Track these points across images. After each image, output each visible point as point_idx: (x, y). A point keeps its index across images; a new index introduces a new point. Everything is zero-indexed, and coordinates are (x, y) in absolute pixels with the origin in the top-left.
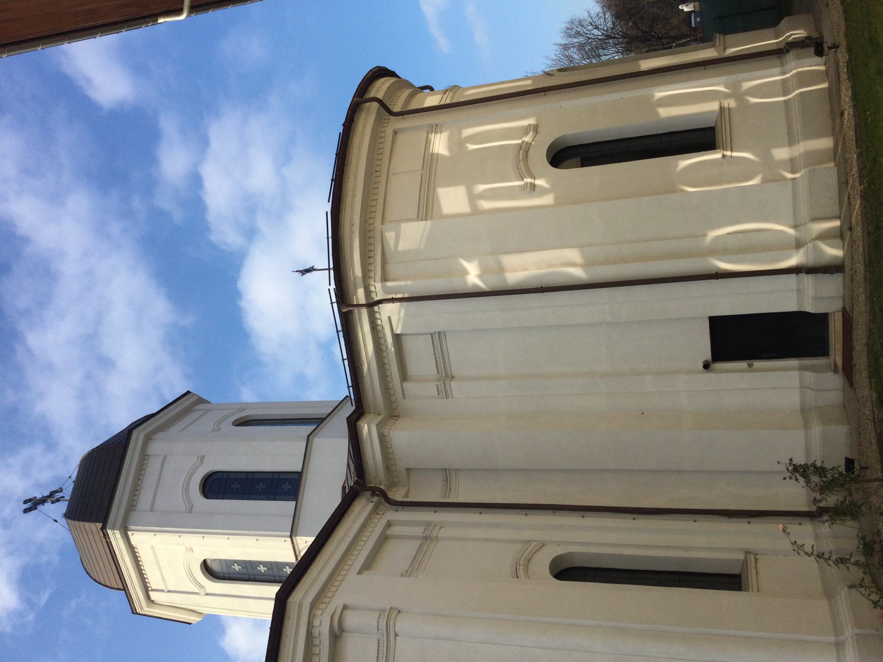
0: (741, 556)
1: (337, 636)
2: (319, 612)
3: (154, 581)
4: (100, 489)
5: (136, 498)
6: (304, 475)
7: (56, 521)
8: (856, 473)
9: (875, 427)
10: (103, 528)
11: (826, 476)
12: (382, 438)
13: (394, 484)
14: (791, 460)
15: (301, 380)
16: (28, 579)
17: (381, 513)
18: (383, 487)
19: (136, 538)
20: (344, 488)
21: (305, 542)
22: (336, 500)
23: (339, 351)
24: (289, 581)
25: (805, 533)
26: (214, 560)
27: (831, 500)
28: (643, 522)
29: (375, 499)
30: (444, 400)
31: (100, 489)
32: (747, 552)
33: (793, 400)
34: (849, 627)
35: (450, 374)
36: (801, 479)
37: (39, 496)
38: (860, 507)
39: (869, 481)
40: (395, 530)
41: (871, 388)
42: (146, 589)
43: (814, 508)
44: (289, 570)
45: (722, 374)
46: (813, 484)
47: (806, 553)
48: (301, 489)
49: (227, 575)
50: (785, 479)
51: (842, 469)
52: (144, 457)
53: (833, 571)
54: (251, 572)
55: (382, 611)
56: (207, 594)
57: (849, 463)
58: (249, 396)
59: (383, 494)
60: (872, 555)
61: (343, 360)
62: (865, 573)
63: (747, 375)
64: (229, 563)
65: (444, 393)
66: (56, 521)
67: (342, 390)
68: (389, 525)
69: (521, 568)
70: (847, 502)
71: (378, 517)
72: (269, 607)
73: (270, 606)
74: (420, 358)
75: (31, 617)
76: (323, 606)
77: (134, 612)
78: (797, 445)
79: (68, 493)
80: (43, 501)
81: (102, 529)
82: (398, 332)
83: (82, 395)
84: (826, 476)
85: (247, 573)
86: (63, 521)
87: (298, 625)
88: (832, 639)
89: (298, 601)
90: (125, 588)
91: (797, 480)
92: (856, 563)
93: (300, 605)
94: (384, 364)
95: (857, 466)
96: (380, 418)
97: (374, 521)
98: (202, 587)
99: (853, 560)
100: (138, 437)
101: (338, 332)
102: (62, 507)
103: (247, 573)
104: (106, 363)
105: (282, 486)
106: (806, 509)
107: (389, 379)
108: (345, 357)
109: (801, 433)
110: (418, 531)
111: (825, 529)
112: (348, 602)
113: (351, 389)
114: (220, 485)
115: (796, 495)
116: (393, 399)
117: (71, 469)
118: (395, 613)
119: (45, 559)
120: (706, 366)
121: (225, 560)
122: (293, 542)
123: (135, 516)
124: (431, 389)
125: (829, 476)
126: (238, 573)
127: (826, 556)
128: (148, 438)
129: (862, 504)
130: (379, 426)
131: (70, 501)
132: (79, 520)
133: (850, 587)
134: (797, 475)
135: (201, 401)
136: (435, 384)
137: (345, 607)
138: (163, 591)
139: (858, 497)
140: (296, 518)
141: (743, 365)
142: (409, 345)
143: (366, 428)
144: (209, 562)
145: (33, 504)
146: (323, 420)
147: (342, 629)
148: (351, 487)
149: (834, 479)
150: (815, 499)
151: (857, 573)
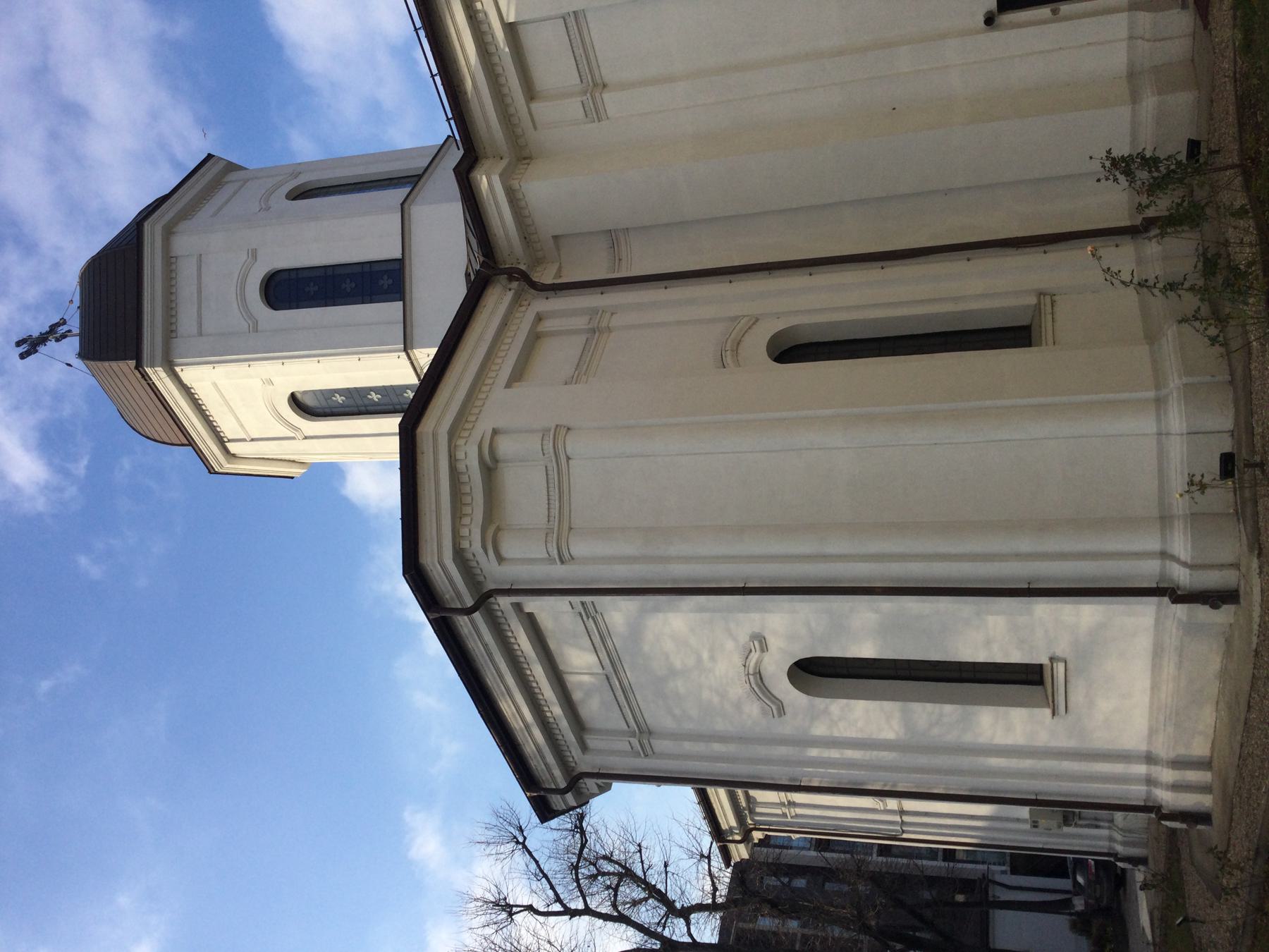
0: (1032, 300)
1: (490, 468)
2: (461, 442)
3: (228, 428)
4: (118, 310)
5: (174, 320)
6: (407, 262)
7: (69, 365)
8: (1202, 160)
9: (1235, 86)
10: (139, 366)
11: (1157, 170)
12: (511, 195)
13: (538, 261)
14: (1109, 152)
15: (374, 110)
16: (52, 441)
17: (525, 303)
18: (523, 267)
19: (189, 374)
20: (467, 275)
21: (425, 356)
22: (459, 292)
23: (423, 60)
24: (413, 409)
25: (1122, 256)
26: (305, 392)
27: (1162, 206)
28: (896, 271)
29: (515, 285)
30: (596, 124)
31: (118, 310)
32: (1041, 294)
33: (1116, 59)
34: (1175, 375)
35: (599, 81)
36: (1122, 178)
37: (36, 334)
38: (1203, 208)
39: (1220, 169)
40: (547, 325)
41: (1235, 26)
42: (221, 441)
43: (1138, 221)
44: (411, 395)
45: (1015, 31)
46: (1139, 183)
47: (1123, 283)
48: (407, 284)
49: (328, 411)
50: (1099, 180)
51: (1183, 157)
52: (170, 261)
53: (1158, 303)
54: (360, 402)
55: (545, 432)
56: (306, 438)
57: (1194, 146)
58: (304, 148)
59: (525, 277)
60: (1214, 274)
61: (433, 76)
62: (1202, 300)
63: (1054, 26)
64: (329, 394)
65: (595, 113)
66: (69, 365)
67: (439, 128)
68: (539, 318)
69: (728, 354)
70: (1185, 204)
71: (523, 309)
72: (392, 446)
73: (395, 443)
74: (553, 63)
75: (72, 491)
76: (466, 434)
77: (211, 471)
78: (1118, 130)
79: (74, 324)
80: (43, 339)
81: (137, 368)
82: (511, 20)
83: (52, 166)
84: (1157, 170)
85: (355, 404)
86: (77, 363)
87: (435, 453)
88: (1151, 394)
89: (430, 431)
90: (191, 443)
91: (1116, 180)
92: (1192, 289)
93: (435, 435)
94: (497, 76)
95: (1204, 151)
96: (503, 163)
97: (518, 315)
98: (297, 429)
99: (1187, 285)
100: (153, 233)
101: (416, 30)
102: (73, 344)
103: (355, 404)
104: (74, 113)
105: (378, 282)
106: (1127, 223)
107: (509, 100)
108: (435, 71)
109: (1125, 111)
110: (581, 322)
111: (1152, 248)
112: (500, 424)
113: (452, 122)
114: (289, 289)
115: (1113, 203)
116: (519, 131)
117: (69, 280)
118: (563, 431)
119: (67, 411)
120: (989, 20)
121: (321, 391)
122: (409, 358)
123: (179, 344)
124: (573, 108)
125: (1162, 169)
126: (342, 406)
127: (1151, 283)
128: (169, 232)
129: (1207, 204)
130: (505, 177)
131: (82, 336)
132: (101, 359)
133: (1180, 322)
134: (1117, 173)
135: (232, 167)
136: (579, 99)
137: (495, 432)
138: (244, 440)
139: (1201, 194)
140: (406, 222)
141: (1044, 12)
142: (529, 38)
143: (487, 182)
144: (299, 396)
145: (30, 346)
146: (420, 177)
147: (495, 460)
148: (478, 272)
149: (1170, 172)
150: (1140, 205)
151: (1190, 302)
